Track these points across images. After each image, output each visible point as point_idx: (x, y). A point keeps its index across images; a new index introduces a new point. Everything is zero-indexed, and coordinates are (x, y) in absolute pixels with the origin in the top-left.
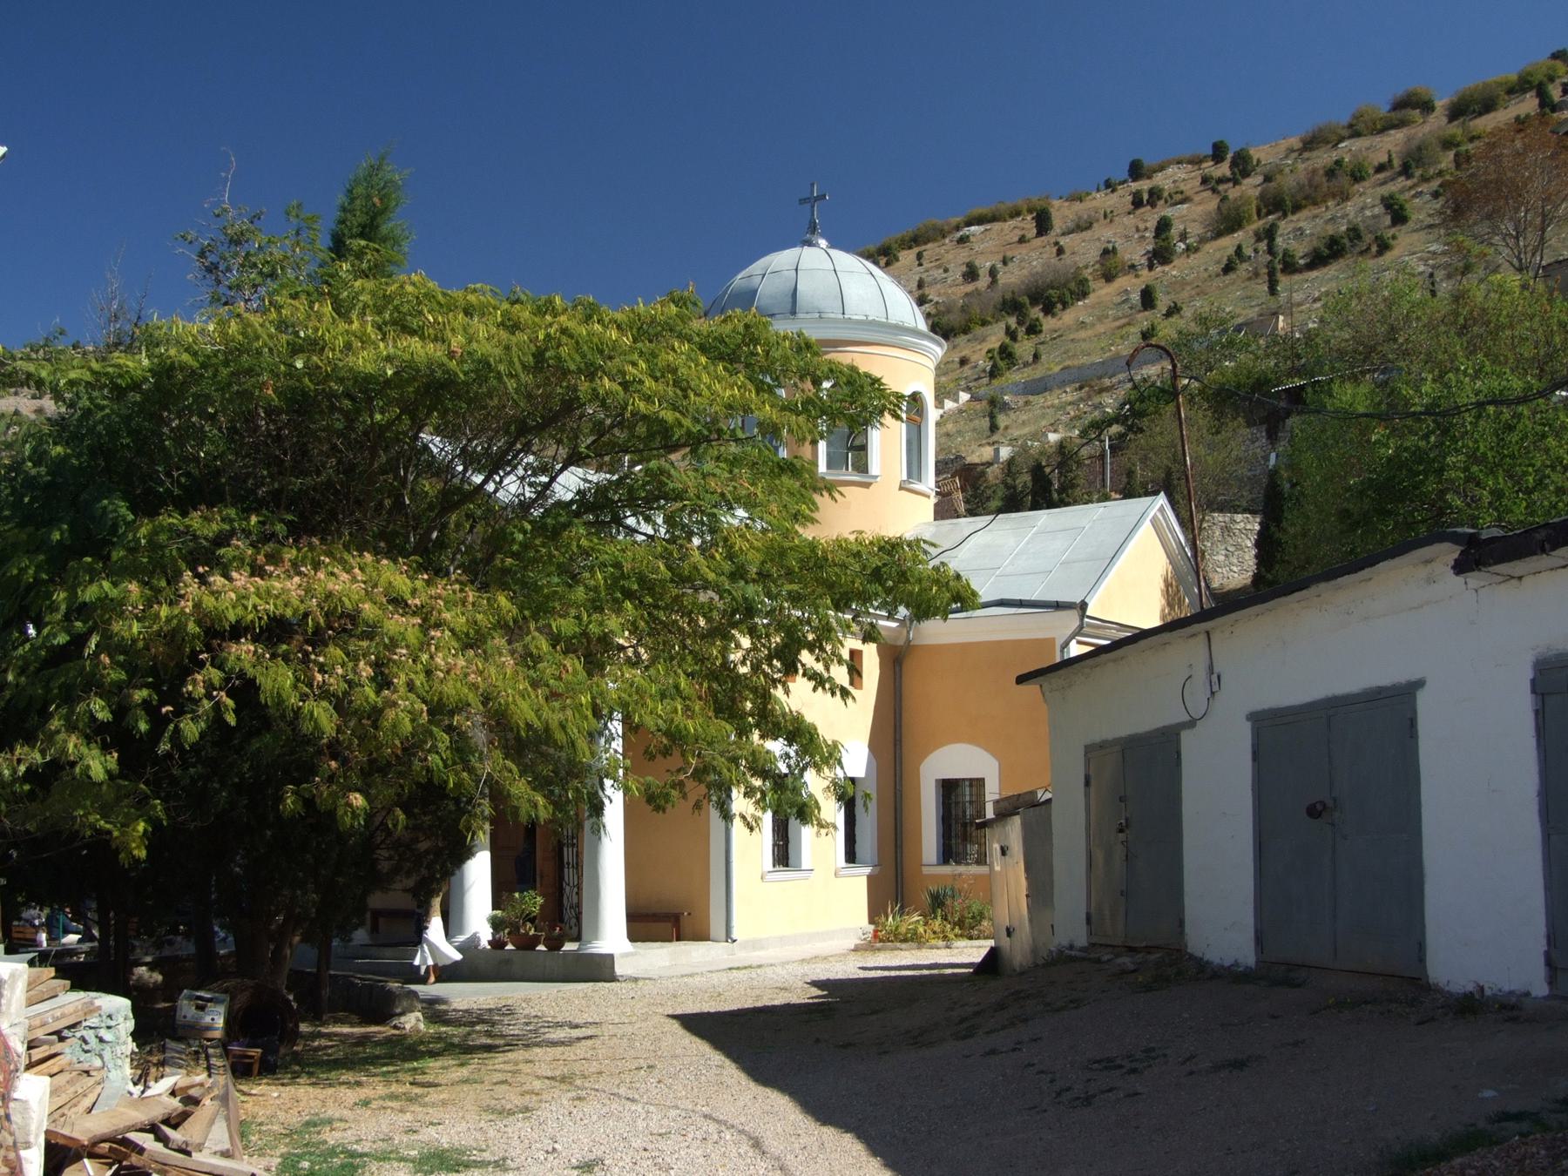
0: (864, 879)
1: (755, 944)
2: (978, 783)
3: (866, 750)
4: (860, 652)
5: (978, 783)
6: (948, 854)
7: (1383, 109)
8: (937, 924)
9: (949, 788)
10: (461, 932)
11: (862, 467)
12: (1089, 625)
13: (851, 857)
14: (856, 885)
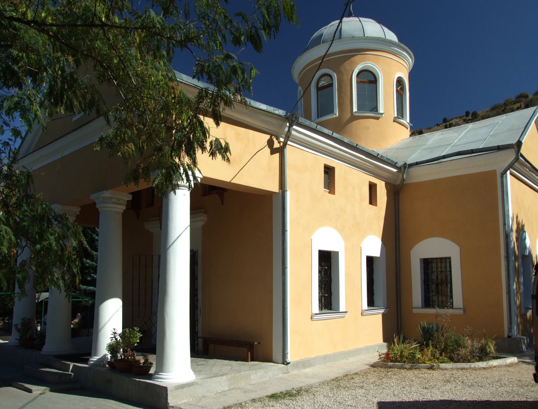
0: (380, 316)
1: (305, 364)
2: (447, 261)
3: (381, 242)
4: (375, 185)
5: (447, 261)
6: (427, 303)
7: (514, 99)
8: (429, 351)
9: (426, 263)
10: (96, 355)
11: (375, 109)
12: (522, 164)
13: (371, 303)
14: (375, 321)
